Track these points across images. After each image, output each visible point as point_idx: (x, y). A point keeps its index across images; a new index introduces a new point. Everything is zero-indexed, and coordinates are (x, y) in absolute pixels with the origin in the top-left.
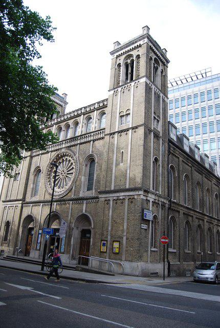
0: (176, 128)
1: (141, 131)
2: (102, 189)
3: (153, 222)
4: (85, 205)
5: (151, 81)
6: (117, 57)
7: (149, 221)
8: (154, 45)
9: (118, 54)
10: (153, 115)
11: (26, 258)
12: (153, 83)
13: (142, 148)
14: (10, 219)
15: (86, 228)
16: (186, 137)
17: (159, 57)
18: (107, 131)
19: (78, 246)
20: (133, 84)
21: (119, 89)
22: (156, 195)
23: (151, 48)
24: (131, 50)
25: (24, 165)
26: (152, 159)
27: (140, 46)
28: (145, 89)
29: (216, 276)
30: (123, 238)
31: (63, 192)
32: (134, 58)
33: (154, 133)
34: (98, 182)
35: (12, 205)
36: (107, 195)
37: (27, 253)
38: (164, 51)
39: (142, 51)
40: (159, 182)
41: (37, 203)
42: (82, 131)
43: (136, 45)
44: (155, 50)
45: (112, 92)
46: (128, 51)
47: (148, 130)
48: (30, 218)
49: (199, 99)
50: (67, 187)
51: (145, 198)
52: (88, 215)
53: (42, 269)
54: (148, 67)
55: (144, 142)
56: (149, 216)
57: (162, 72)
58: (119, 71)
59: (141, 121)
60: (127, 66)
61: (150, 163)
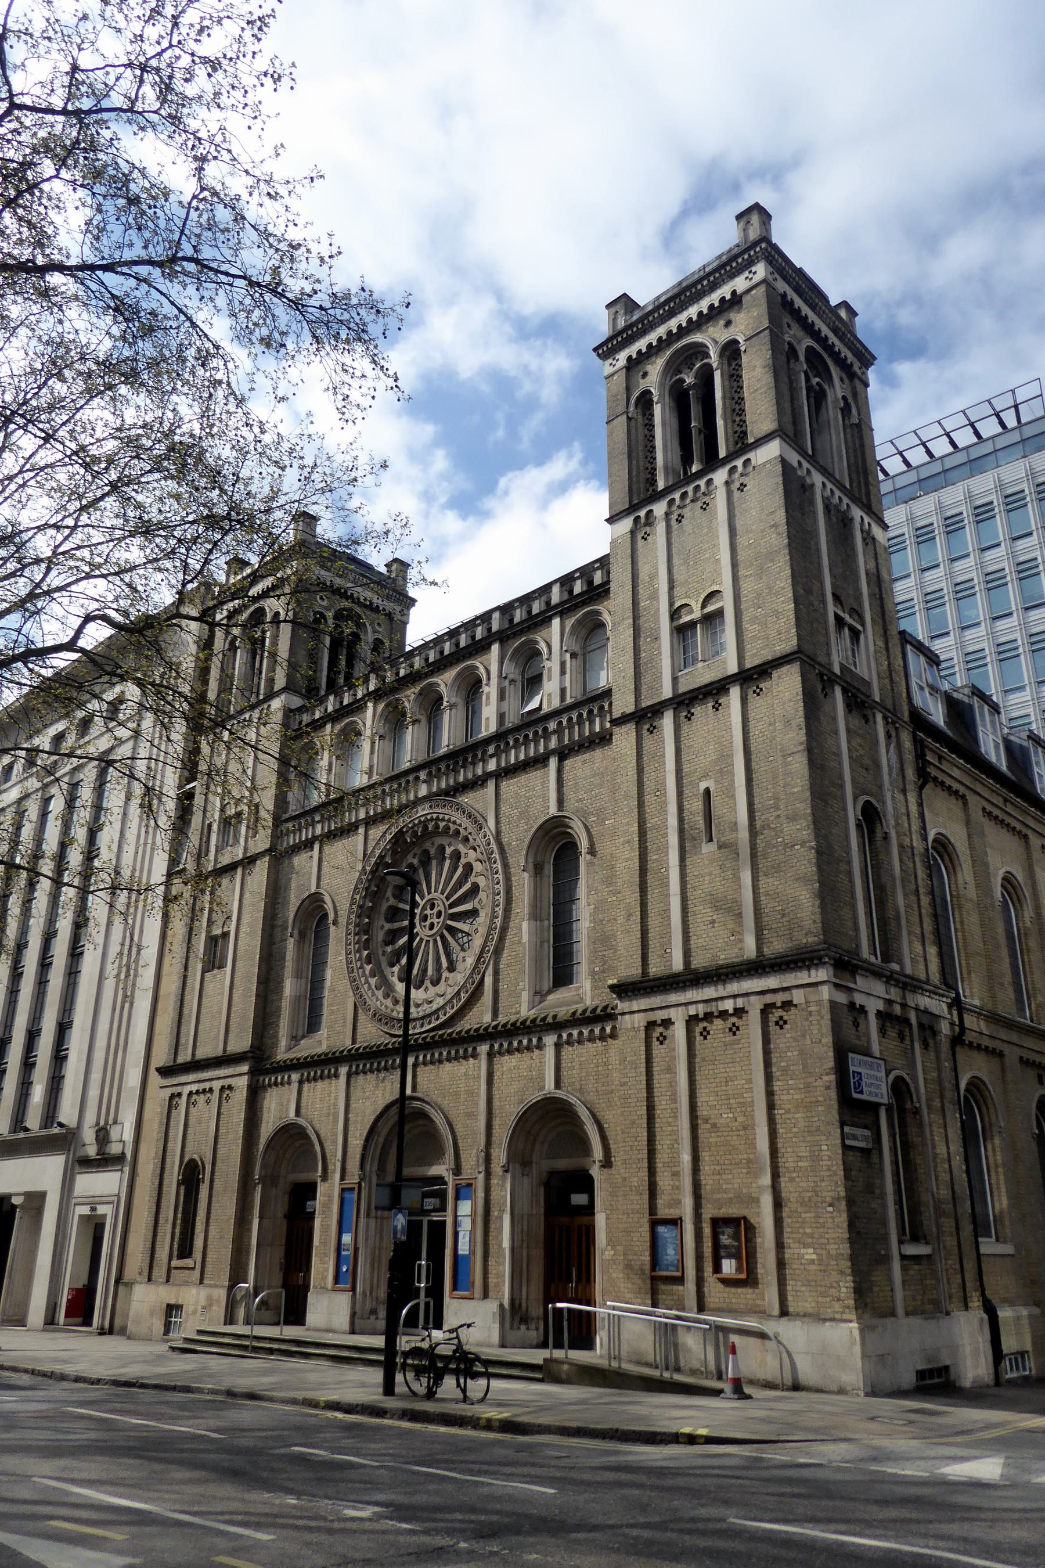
0: (933, 660)
1: (787, 687)
2: (629, 969)
3: (889, 1109)
4: (550, 1052)
5: (801, 451)
6: (634, 365)
7: (878, 1105)
8: (797, 290)
9: (632, 350)
10: (831, 608)
11: (291, 1332)
12: (813, 459)
13: (799, 764)
14: (200, 1148)
15: (563, 1164)
16: (985, 698)
17: (823, 341)
18: (623, 703)
19: (538, 1253)
20: (720, 476)
21: (659, 508)
22: (890, 979)
23: (787, 305)
24: (693, 326)
25: (247, 895)
26: (852, 814)
27: (736, 301)
28: (781, 489)
29: (1006, 1465)
30: (757, 1201)
31: (440, 1002)
32: (714, 359)
33: (845, 691)
34: (603, 940)
35: (207, 1085)
36: (656, 1001)
37: (296, 1314)
38: (843, 314)
39: (743, 325)
40: (898, 918)
41: (322, 1065)
42: (563, 691)
43: (714, 298)
44: (806, 310)
45: (627, 524)
46: (682, 332)
47: (819, 681)
48: (294, 1138)
49: (940, 549)
50: (459, 978)
51: (842, 998)
52: (573, 1100)
53: (389, 1388)
54: (785, 389)
55: (809, 734)
56: (875, 1087)
57: (846, 410)
58: (650, 426)
59: (775, 630)
60: (679, 397)
61: (847, 829)
